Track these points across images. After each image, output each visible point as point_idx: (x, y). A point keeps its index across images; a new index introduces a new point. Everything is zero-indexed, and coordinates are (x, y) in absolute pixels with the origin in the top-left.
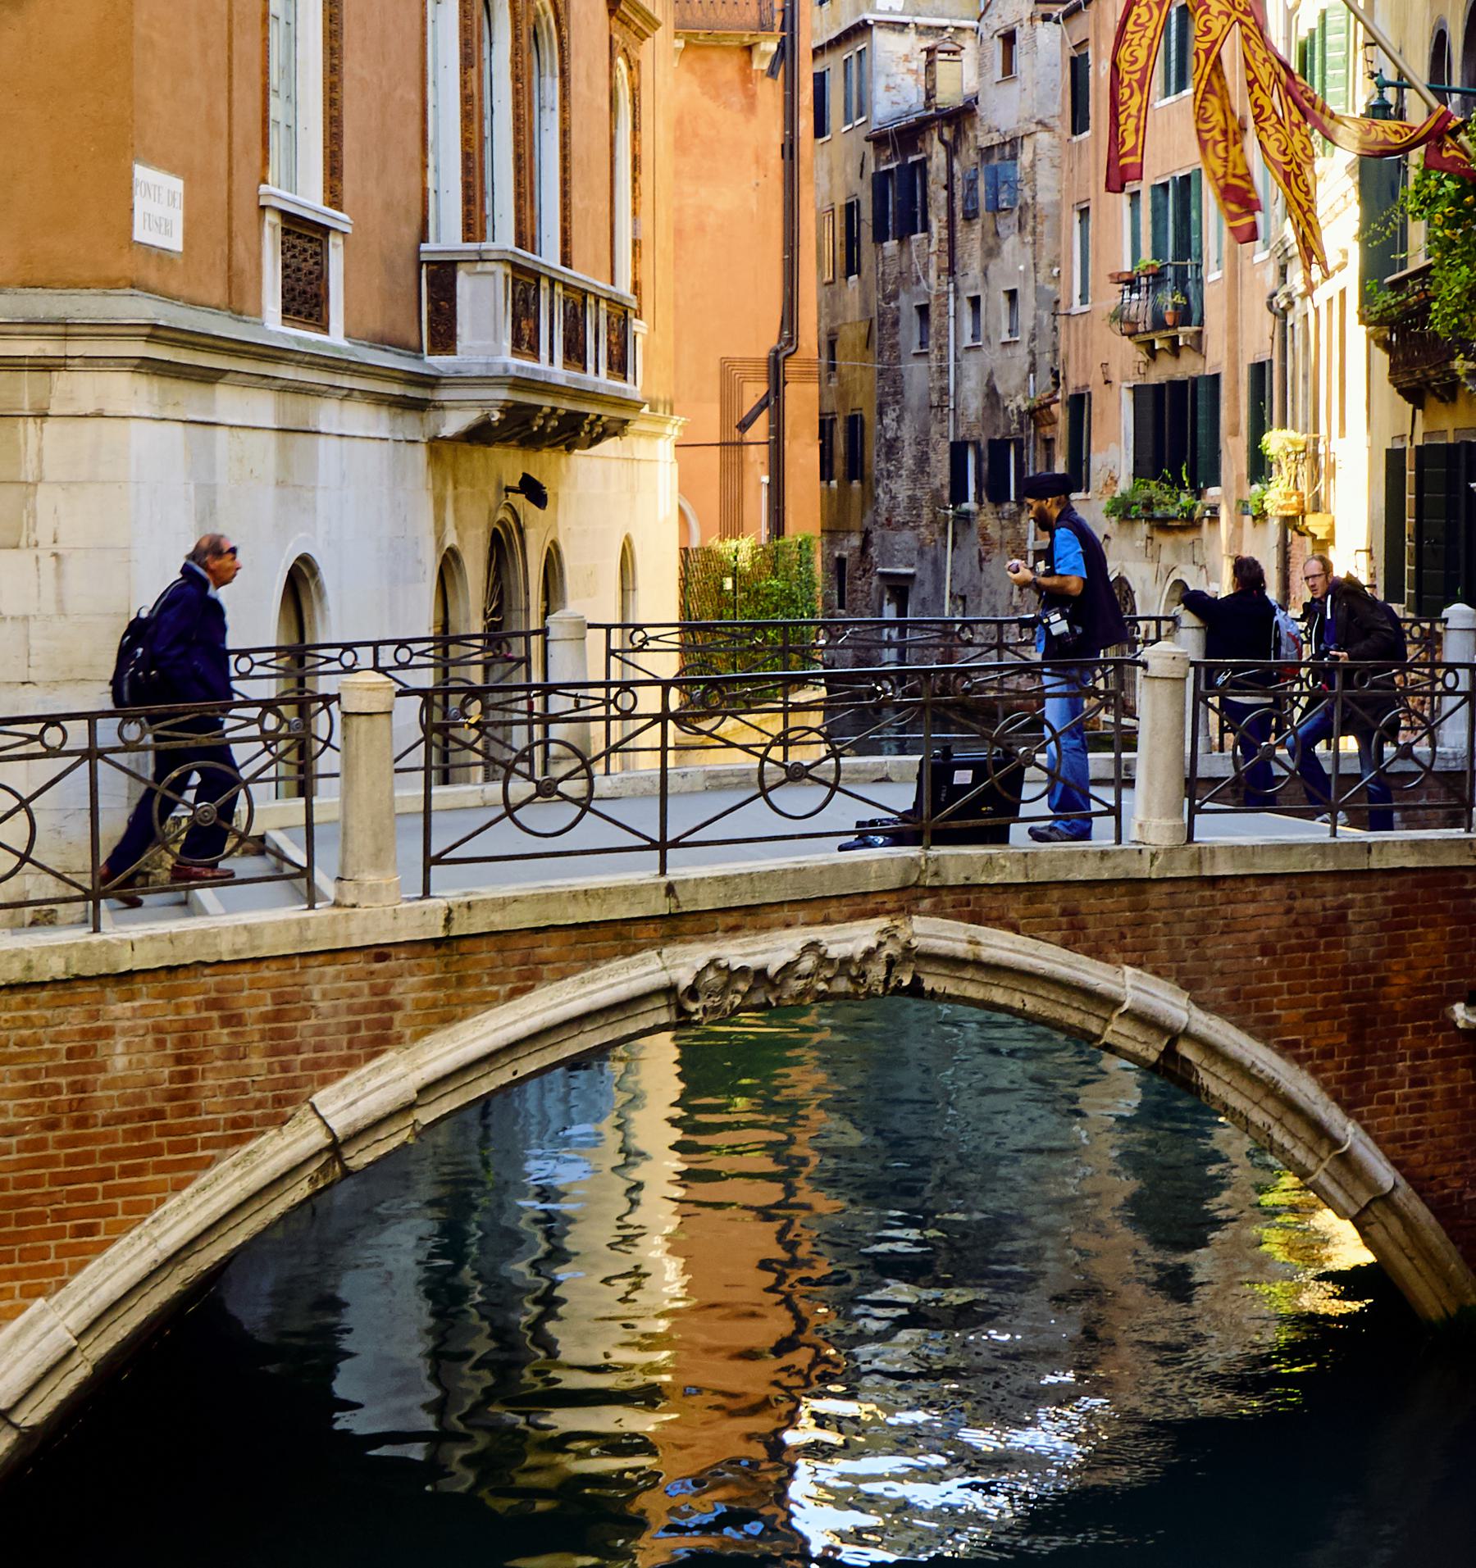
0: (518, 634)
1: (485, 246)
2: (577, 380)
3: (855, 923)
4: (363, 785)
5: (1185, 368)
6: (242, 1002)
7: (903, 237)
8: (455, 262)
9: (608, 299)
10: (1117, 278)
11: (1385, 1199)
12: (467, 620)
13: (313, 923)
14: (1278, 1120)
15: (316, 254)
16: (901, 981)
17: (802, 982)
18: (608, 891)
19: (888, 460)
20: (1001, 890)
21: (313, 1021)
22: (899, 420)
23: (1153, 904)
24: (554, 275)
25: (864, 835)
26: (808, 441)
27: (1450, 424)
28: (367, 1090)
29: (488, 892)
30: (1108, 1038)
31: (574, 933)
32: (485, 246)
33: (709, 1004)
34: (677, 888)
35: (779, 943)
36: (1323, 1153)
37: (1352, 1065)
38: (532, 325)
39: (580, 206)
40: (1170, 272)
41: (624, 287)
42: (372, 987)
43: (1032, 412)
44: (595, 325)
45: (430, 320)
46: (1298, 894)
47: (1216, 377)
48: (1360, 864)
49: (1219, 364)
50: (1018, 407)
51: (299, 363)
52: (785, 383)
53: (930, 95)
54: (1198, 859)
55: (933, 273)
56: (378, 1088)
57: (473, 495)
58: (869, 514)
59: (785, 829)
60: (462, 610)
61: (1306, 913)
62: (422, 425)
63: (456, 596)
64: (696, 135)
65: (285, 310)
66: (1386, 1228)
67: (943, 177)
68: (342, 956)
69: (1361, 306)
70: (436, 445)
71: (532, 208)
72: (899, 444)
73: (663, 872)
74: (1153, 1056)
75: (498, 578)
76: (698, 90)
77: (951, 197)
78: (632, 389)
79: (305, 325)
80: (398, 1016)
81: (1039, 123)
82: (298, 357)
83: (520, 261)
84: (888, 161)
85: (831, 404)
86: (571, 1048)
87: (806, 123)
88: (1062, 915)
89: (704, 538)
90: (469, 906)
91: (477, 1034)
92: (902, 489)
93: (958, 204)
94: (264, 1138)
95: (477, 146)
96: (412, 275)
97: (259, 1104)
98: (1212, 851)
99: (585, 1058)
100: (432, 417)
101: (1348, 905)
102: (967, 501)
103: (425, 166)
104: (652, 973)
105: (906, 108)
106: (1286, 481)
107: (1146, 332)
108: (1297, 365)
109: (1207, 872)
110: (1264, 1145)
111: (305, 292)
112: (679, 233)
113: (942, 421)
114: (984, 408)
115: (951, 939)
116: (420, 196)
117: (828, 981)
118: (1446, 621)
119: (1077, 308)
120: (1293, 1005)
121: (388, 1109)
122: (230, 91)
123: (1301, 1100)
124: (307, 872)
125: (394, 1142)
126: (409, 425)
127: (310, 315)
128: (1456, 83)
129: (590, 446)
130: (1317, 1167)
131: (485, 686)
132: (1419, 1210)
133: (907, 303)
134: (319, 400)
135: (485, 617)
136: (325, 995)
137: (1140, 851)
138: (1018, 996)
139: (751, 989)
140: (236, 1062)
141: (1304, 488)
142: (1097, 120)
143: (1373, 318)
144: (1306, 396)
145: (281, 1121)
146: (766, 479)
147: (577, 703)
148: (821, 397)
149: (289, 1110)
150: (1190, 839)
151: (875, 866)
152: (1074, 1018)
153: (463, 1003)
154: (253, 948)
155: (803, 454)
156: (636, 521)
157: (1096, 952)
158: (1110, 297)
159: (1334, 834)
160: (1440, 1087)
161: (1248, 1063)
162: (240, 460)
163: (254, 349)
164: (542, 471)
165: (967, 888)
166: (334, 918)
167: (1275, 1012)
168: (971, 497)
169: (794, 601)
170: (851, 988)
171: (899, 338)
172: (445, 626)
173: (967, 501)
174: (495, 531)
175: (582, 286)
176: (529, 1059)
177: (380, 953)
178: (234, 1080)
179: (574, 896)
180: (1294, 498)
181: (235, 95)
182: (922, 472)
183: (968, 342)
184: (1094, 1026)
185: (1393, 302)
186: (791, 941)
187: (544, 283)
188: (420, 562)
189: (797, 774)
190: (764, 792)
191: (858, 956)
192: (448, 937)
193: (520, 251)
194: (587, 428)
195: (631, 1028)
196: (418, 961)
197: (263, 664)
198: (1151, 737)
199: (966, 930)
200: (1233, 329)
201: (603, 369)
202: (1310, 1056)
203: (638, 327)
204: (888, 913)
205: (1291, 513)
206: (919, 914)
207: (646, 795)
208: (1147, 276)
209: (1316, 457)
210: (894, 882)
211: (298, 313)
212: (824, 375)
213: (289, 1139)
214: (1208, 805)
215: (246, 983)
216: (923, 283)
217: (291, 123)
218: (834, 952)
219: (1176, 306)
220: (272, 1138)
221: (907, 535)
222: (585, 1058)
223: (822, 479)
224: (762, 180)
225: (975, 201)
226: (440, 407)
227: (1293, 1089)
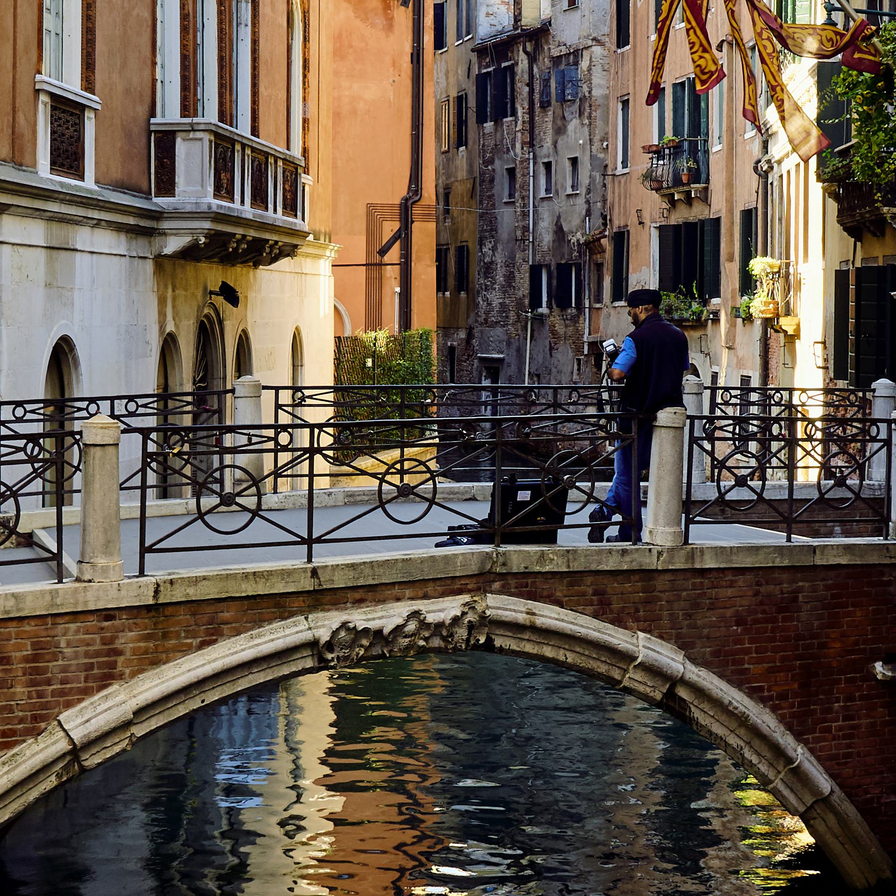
0: (214, 393)
1: (195, 120)
2: (261, 216)
3: (446, 599)
4: (97, 496)
5: (697, 213)
6: (10, 648)
7: (497, 121)
8: (174, 132)
9: (284, 160)
10: (648, 149)
11: (824, 801)
12: (181, 385)
13: (61, 592)
14: (748, 743)
15: (76, 124)
16: (479, 640)
17: (407, 640)
18: (270, 573)
19: (486, 277)
20: (550, 576)
21: (60, 662)
22: (494, 249)
23: (659, 588)
24: (245, 141)
25: (453, 536)
26: (429, 263)
27: (881, 253)
28: (97, 712)
29: (185, 573)
30: (626, 683)
31: (246, 602)
32: (195, 120)
33: (341, 654)
34: (320, 572)
35: (391, 612)
36: (780, 768)
37: (801, 704)
38: (228, 176)
39: (265, 94)
40: (686, 144)
41: (296, 152)
42: (102, 638)
43: (587, 244)
44: (276, 177)
45: (156, 172)
46: (763, 581)
47: (718, 220)
48: (807, 561)
49: (720, 211)
50: (578, 240)
51: (62, 201)
52: (412, 222)
53: (517, 18)
54: (691, 556)
55: (518, 146)
56: (106, 711)
57: (186, 296)
58: (472, 315)
59: (401, 532)
60: (178, 378)
61: (769, 596)
62: (151, 246)
63: (174, 368)
64: (351, 46)
65: (53, 163)
66: (825, 821)
67: (526, 77)
68: (82, 617)
69: (818, 168)
70: (160, 260)
71: (231, 94)
72: (494, 267)
73: (310, 560)
74: (658, 696)
75: (204, 355)
76: (352, 14)
77: (531, 92)
78: (297, 223)
79: (67, 174)
80: (121, 659)
81: (594, 39)
82: (62, 196)
83: (220, 131)
84: (488, 66)
85: (445, 237)
86: (243, 684)
87: (428, 38)
88: (593, 595)
89: (354, 329)
90: (172, 582)
91: (177, 673)
92: (495, 297)
93: (537, 96)
94: (24, 744)
95: (191, 50)
96: (144, 140)
97: (21, 721)
98: (702, 551)
99: (262, 691)
100: (157, 240)
101: (800, 590)
102: (541, 307)
103: (154, 64)
104: (301, 631)
105: (500, 28)
106: (766, 293)
107: (669, 188)
108: (774, 211)
109: (697, 566)
110: (741, 763)
111: (67, 151)
112: (337, 116)
113: (524, 250)
114: (554, 241)
115: (514, 611)
116: (150, 85)
117: (426, 639)
118: (874, 391)
119: (620, 170)
120: (758, 661)
121: (113, 725)
122: (15, 8)
123: (765, 729)
124: (57, 557)
125: (117, 749)
126: (141, 246)
127: (71, 167)
128: (886, 9)
129: (270, 264)
130: (776, 777)
131: (192, 429)
132: (849, 809)
133: (500, 167)
134: (77, 227)
135: (194, 384)
136: (69, 644)
137: (650, 550)
138: (562, 652)
139: (371, 645)
140: (5, 690)
141: (778, 298)
142: (635, 38)
143: (826, 177)
144: (780, 234)
145: (36, 733)
146: (398, 290)
147: (250, 440)
148: (438, 233)
149: (43, 725)
150: (686, 542)
151: (461, 558)
152: (603, 668)
153: (166, 651)
154: (18, 610)
155: (425, 272)
156: (304, 314)
157: (618, 622)
158: (642, 163)
159: (789, 539)
160: (864, 721)
161: (726, 702)
162: (20, 269)
163: (30, 190)
164: (236, 281)
165: (526, 574)
166: (76, 589)
167: (746, 666)
168: (544, 304)
169: (417, 376)
170: (443, 644)
171: (494, 191)
172: (166, 387)
173: (541, 307)
174: (202, 321)
175: (265, 149)
176: (212, 692)
177: (108, 614)
178: (4, 703)
179: (246, 576)
180: (771, 305)
181: (19, 11)
182: (510, 286)
183: (543, 194)
184: (616, 674)
185: (840, 165)
186: (400, 610)
187: (238, 147)
188: (147, 343)
189: (405, 492)
190: (382, 505)
191: (448, 622)
192: (156, 604)
193: (221, 124)
194: (268, 250)
195: (285, 670)
196: (135, 621)
197: (33, 412)
198: (659, 469)
199: (527, 604)
200: (730, 185)
201: (280, 209)
202: (771, 698)
203: (306, 179)
204: (469, 591)
205: (769, 316)
206: (491, 592)
207: (301, 508)
208: (669, 148)
209: (788, 274)
210: (473, 569)
211: (62, 165)
212: (441, 217)
213: (42, 746)
214: (698, 518)
215: (13, 635)
216: (512, 153)
217: (59, 32)
218: (431, 618)
219: (689, 169)
220: (30, 745)
221: (499, 331)
222: (262, 691)
223: (438, 290)
224: (397, 79)
225: (549, 94)
226: (163, 234)
227: (759, 721)
